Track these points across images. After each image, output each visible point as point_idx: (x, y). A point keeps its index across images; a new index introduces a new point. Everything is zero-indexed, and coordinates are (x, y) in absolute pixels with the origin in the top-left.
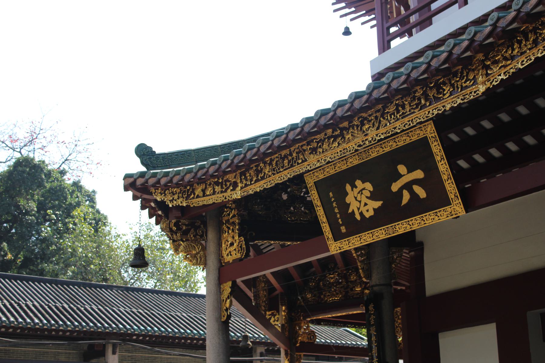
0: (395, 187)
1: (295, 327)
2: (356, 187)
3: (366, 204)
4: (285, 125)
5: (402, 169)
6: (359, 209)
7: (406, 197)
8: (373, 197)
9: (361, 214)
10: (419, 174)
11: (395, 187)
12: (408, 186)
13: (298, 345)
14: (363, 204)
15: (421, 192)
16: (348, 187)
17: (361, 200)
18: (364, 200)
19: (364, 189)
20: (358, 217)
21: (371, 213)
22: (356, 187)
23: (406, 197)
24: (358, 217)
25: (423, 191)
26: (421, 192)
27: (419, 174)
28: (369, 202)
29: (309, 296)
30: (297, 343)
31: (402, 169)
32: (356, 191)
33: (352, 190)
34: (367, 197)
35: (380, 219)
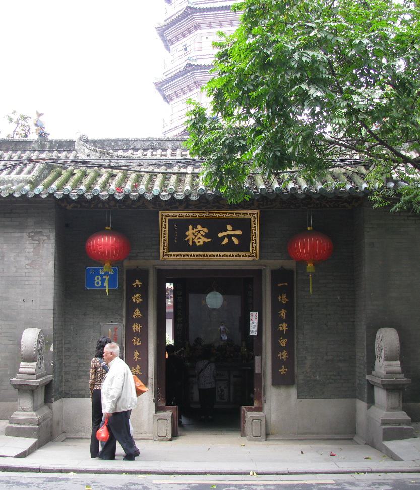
0: (220, 235)
1: (281, 337)
2: (196, 228)
3: (199, 238)
4: (111, 138)
5: (229, 227)
6: (193, 239)
7: (226, 241)
8: (205, 236)
9: (194, 243)
10: (239, 233)
11: (220, 235)
12: (230, 237)
13: (286, 284)
14: (197, 238)
15: (236, 241)
16: (190, 227)
17: (196, 235)
18: (199, 236)
19: (202, 231)
20: (190, 244)
21: (201, 243)
22: (196, 228)
23: (226, 241)
24: (190, 244)
25: (24, 331)
26: (236, 241)
27: (239, 233)
28: (201, 237)
29: (293, 98)
30: (285, 285)
31: (229, 227)
32: (195, 230)
33: (193, 229)
34: (202, 235)
35: (205, 247)
